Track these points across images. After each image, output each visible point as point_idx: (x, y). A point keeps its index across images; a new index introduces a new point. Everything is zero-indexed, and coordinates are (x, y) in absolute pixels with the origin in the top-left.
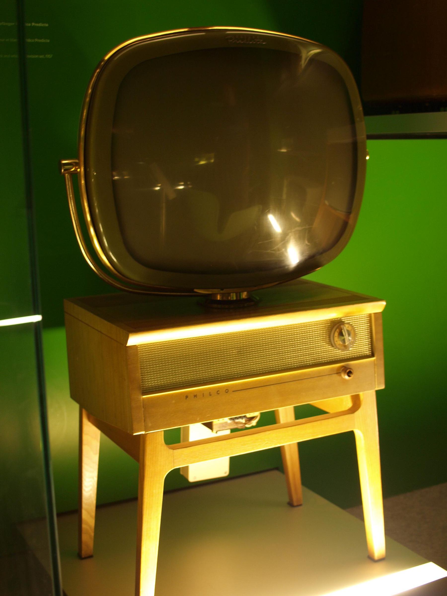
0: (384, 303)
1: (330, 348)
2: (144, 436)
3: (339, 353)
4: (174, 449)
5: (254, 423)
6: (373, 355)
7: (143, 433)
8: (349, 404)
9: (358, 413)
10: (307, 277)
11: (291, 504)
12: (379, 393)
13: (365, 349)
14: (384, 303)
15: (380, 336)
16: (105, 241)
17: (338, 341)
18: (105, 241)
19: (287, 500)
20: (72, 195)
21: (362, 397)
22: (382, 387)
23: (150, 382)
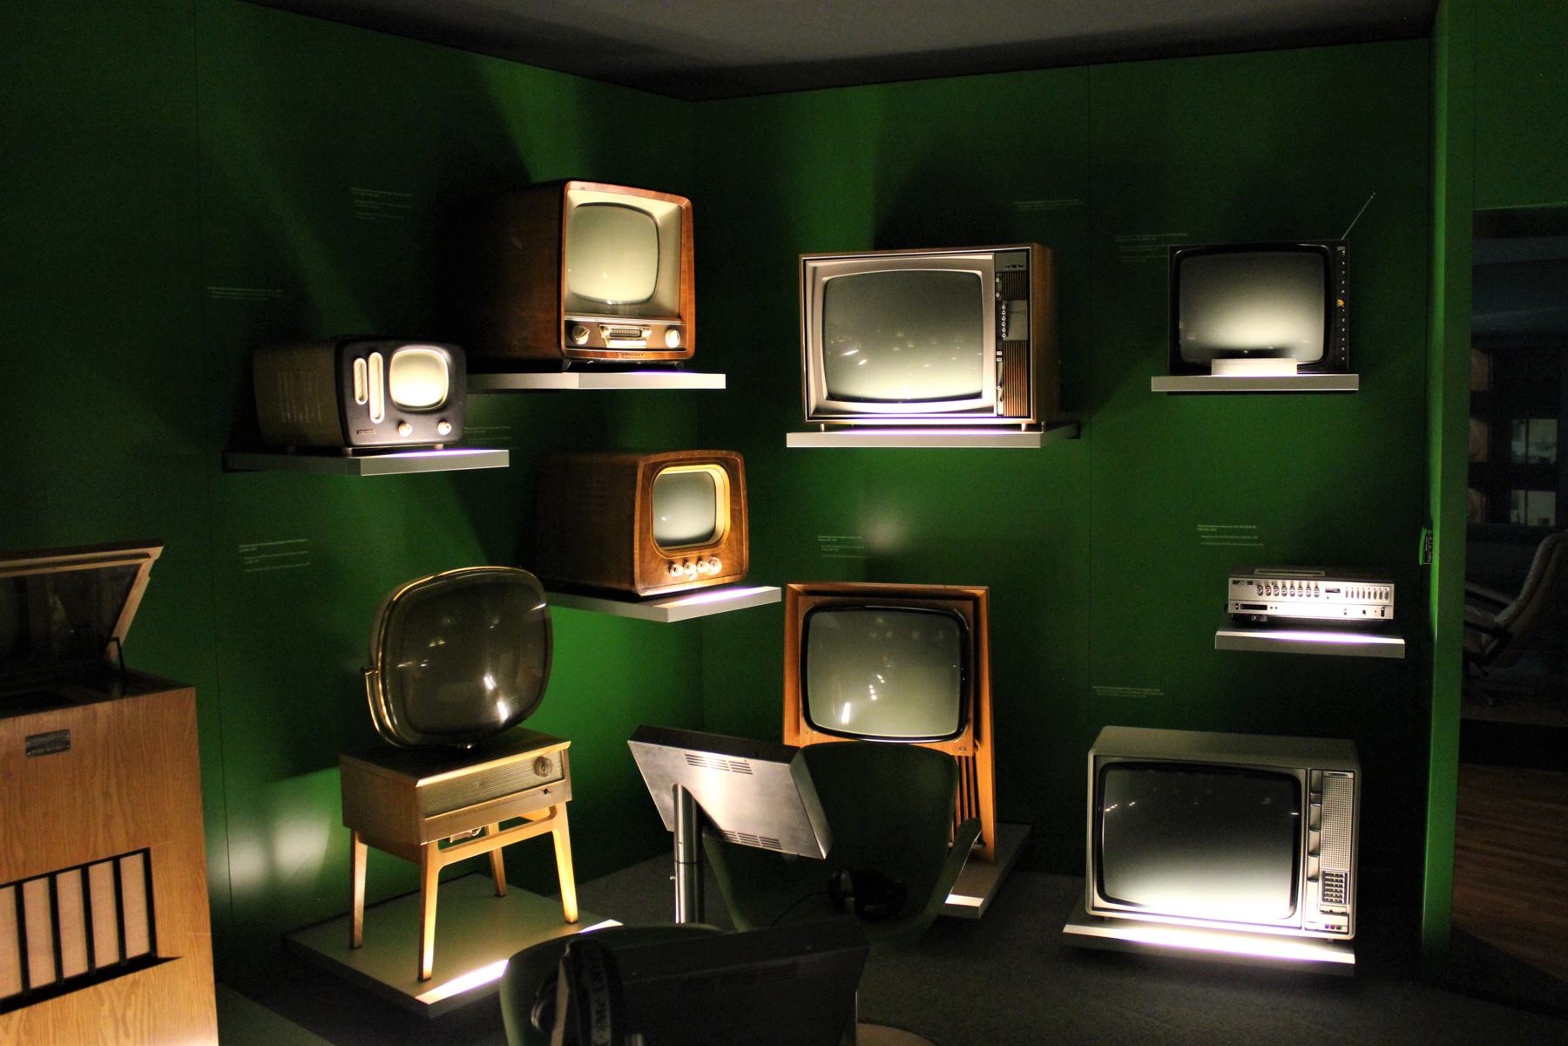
0: (569, 743)
1: (535, 775)
2: (426, 845)
3: (542, 779)
4: (444, 852)
5: (478, 832)
6: (563, 778)
7: (426, 843)
8: (548, 813)
9: (555, 818)
10: (523, 725)
11: (498, 895)
12: (568, 804)
13: (559, 775)
14: (569, 743)
15: (568, 765)
16: (391, 706)
17: (540, 770)
18: (391, 706)
19: (495, 892)
20: (1095, 735)
21: (557, 808)
22: (570, 799)
23: (431, 809)
